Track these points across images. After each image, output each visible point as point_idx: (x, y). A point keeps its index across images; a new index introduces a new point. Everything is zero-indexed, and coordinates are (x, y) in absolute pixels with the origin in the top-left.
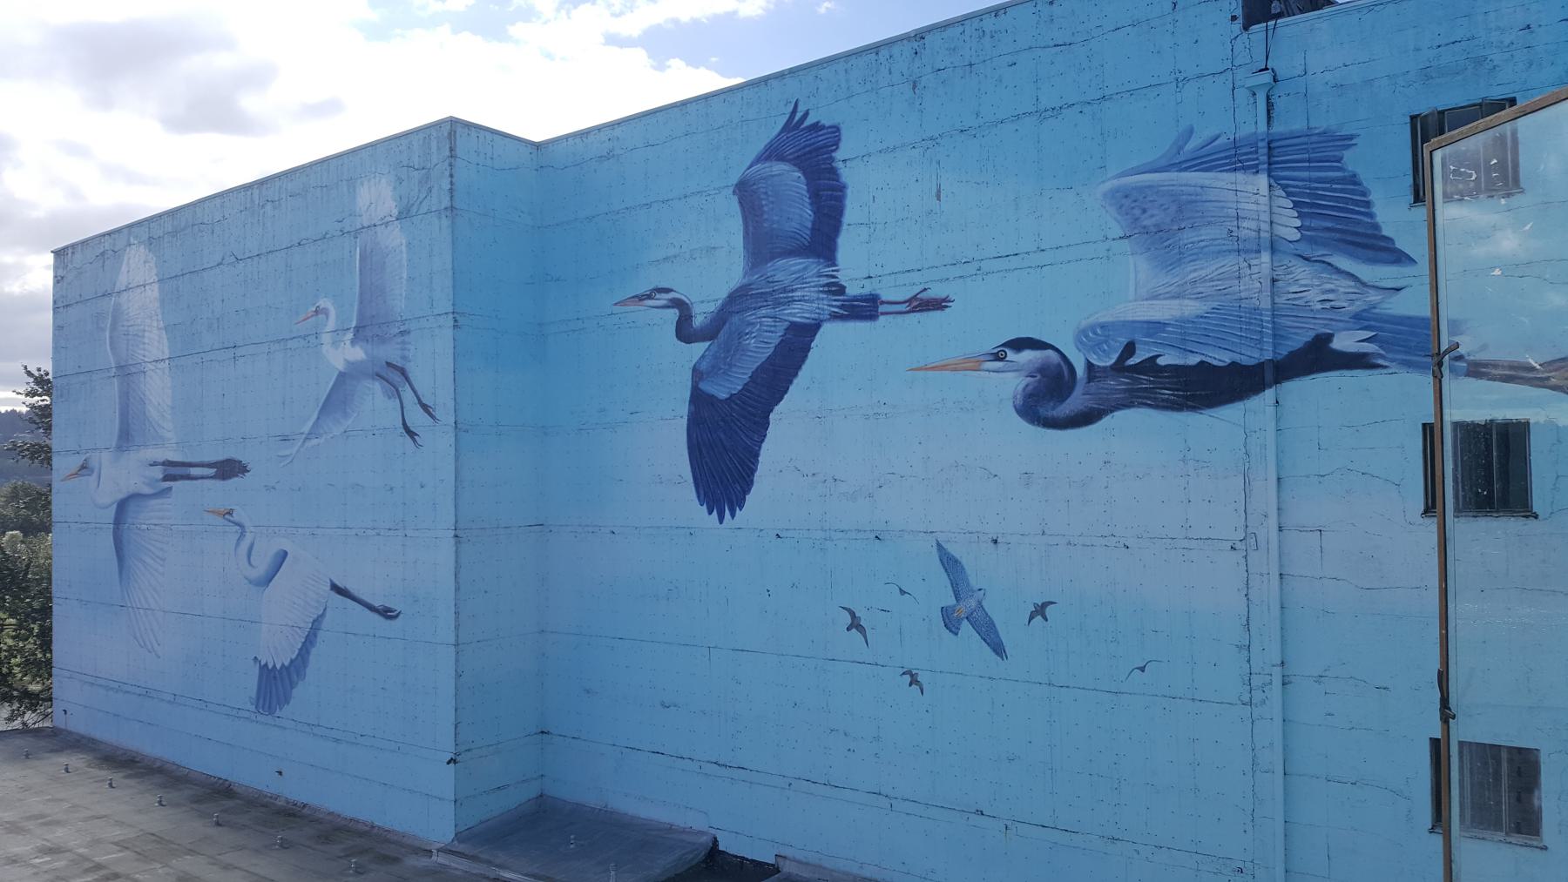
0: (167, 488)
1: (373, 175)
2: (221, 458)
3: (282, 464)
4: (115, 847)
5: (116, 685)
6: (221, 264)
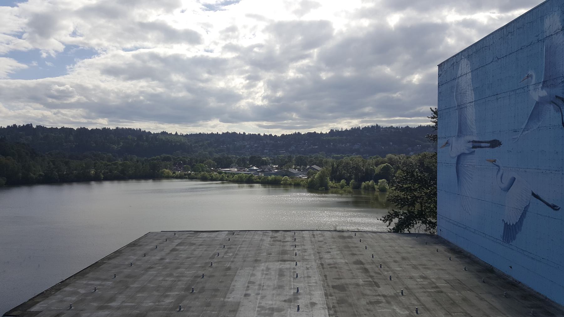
0: (473, 151)
1: (551, 13)
2: (492, 139)
3: (514, 142)
4: (444, 281)
5: (456, 223)
6: (492, 61)
